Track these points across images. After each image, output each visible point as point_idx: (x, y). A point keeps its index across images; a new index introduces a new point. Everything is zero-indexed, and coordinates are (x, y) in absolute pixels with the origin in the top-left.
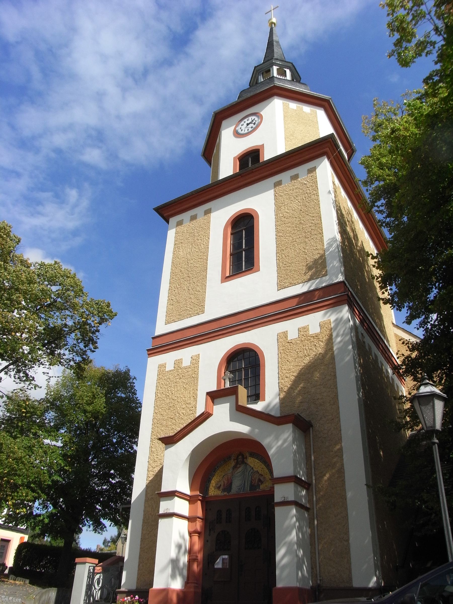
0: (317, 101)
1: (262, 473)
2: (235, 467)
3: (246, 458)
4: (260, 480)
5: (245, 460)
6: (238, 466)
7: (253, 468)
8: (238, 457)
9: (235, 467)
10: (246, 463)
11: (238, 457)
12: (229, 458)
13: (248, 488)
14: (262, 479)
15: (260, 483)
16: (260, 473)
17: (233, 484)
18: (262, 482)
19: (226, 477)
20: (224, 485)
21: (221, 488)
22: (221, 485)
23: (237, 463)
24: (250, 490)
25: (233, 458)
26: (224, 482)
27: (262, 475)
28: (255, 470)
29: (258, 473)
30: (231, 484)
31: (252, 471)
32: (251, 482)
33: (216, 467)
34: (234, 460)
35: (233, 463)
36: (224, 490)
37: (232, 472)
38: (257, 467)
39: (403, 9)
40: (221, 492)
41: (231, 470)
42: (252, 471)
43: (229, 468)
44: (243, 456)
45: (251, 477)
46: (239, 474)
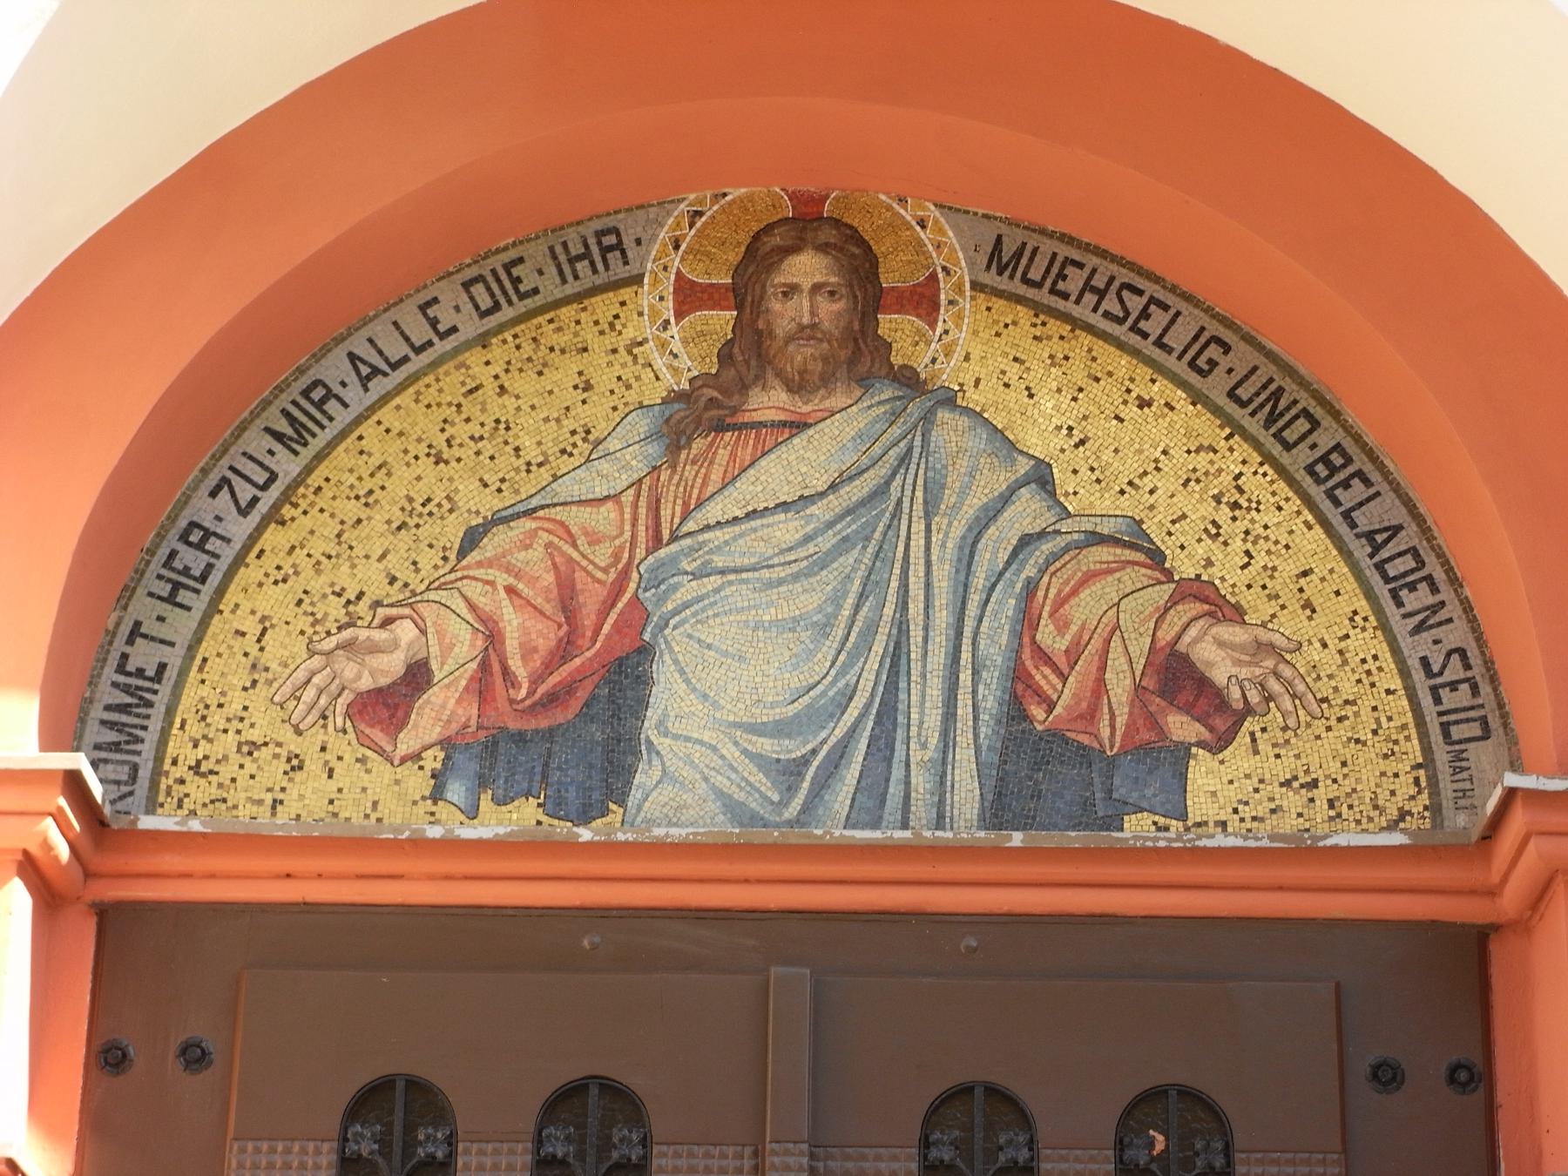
0: (63, 824)
1: (1228, 574)
2: (702, 416)
3: (924, 301)
4: (1175, 677)
5: (895, 326)
6: (768, 402)
7: (1041, 477)
8: (759, 257)
9: (702, 416)
10: (909, 381)
11: (759, 257)
12: (599, 257)
13: (948, 778)
14: (1221, 668)
15: (1181, 727)
16: (1186, 568)
17: (664, 673)
18: (1224, 719)
19: (534, 558)
20: (488, 674)
21: (428, 721)
22: (417, 676)
23: (749, 354)
24: (997, 813)
25: (661, 266)
26: (493, 636)
27: (1219, 607)
28: (1090, 501)
29: (1156, 558)
30: (626, 678)
31: (1027, 512)
32: (1018, 677)
33: (335, 369)
34: (689, 297)
35: (668, 348)
36: (491, 756)
37: (648, 489)
38: (1129, 467)
39: (477, 435)
40: (418, 782)
41: (630, 457)
42: (1027, 512)
43: (596, 413)
44: (859, 261)
45: (1006, 605)
46: (786, 529)
